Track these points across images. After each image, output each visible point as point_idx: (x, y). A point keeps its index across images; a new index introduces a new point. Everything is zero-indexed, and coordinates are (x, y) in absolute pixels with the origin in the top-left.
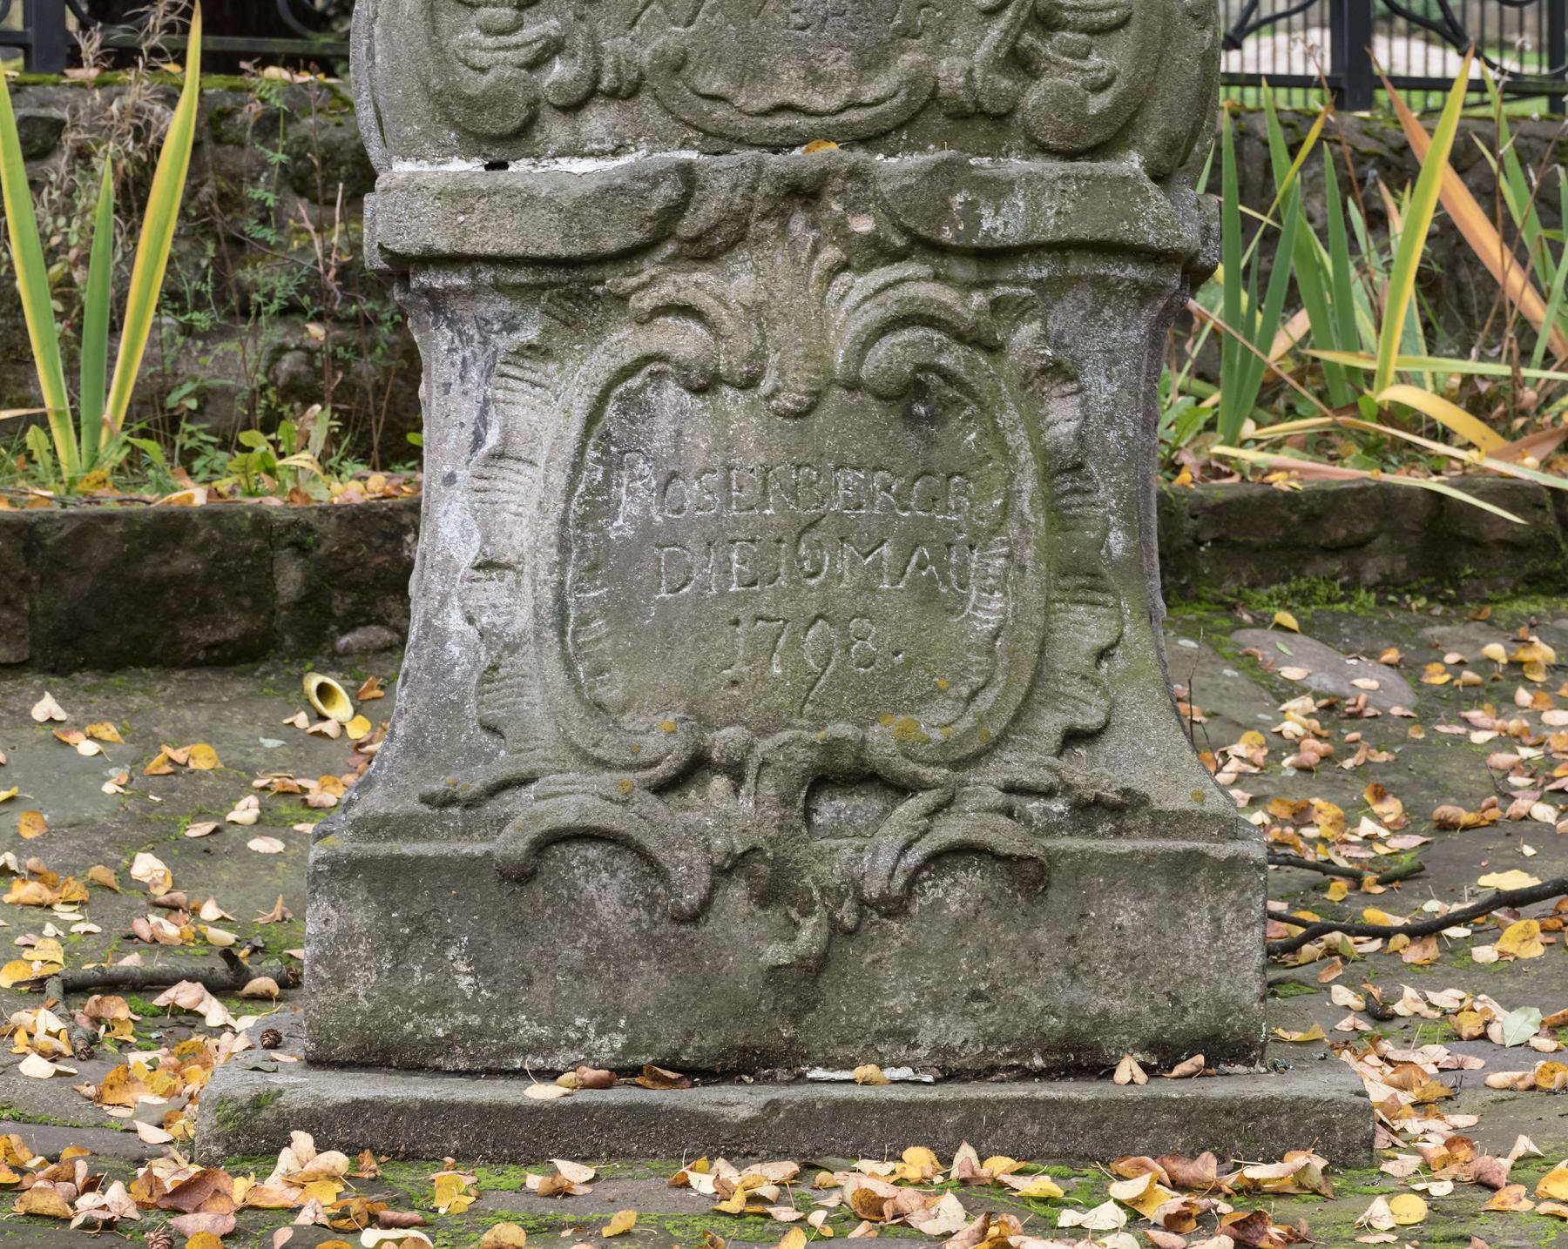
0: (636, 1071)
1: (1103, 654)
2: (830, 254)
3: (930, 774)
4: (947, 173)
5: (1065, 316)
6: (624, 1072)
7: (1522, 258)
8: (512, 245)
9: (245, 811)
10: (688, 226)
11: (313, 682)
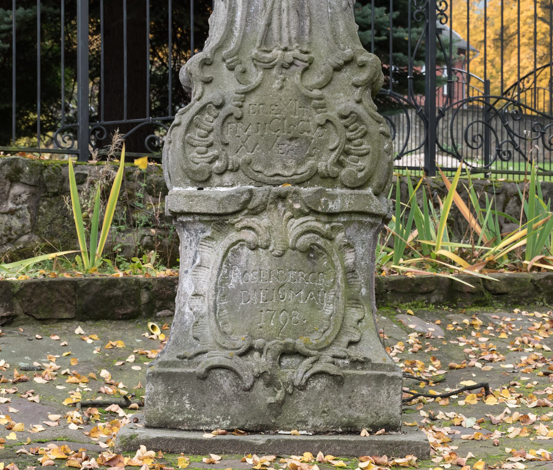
0: (233, 430)
1: (359, 321)
2: (289, 214)
3: (312, 352)
4: (321, 193)
5: (351, 231)
6: (229, 431)
7: (475, 216)
8: (204, 210)
9: (131, 359)
10: (251, 205)
11: (150, 324)
